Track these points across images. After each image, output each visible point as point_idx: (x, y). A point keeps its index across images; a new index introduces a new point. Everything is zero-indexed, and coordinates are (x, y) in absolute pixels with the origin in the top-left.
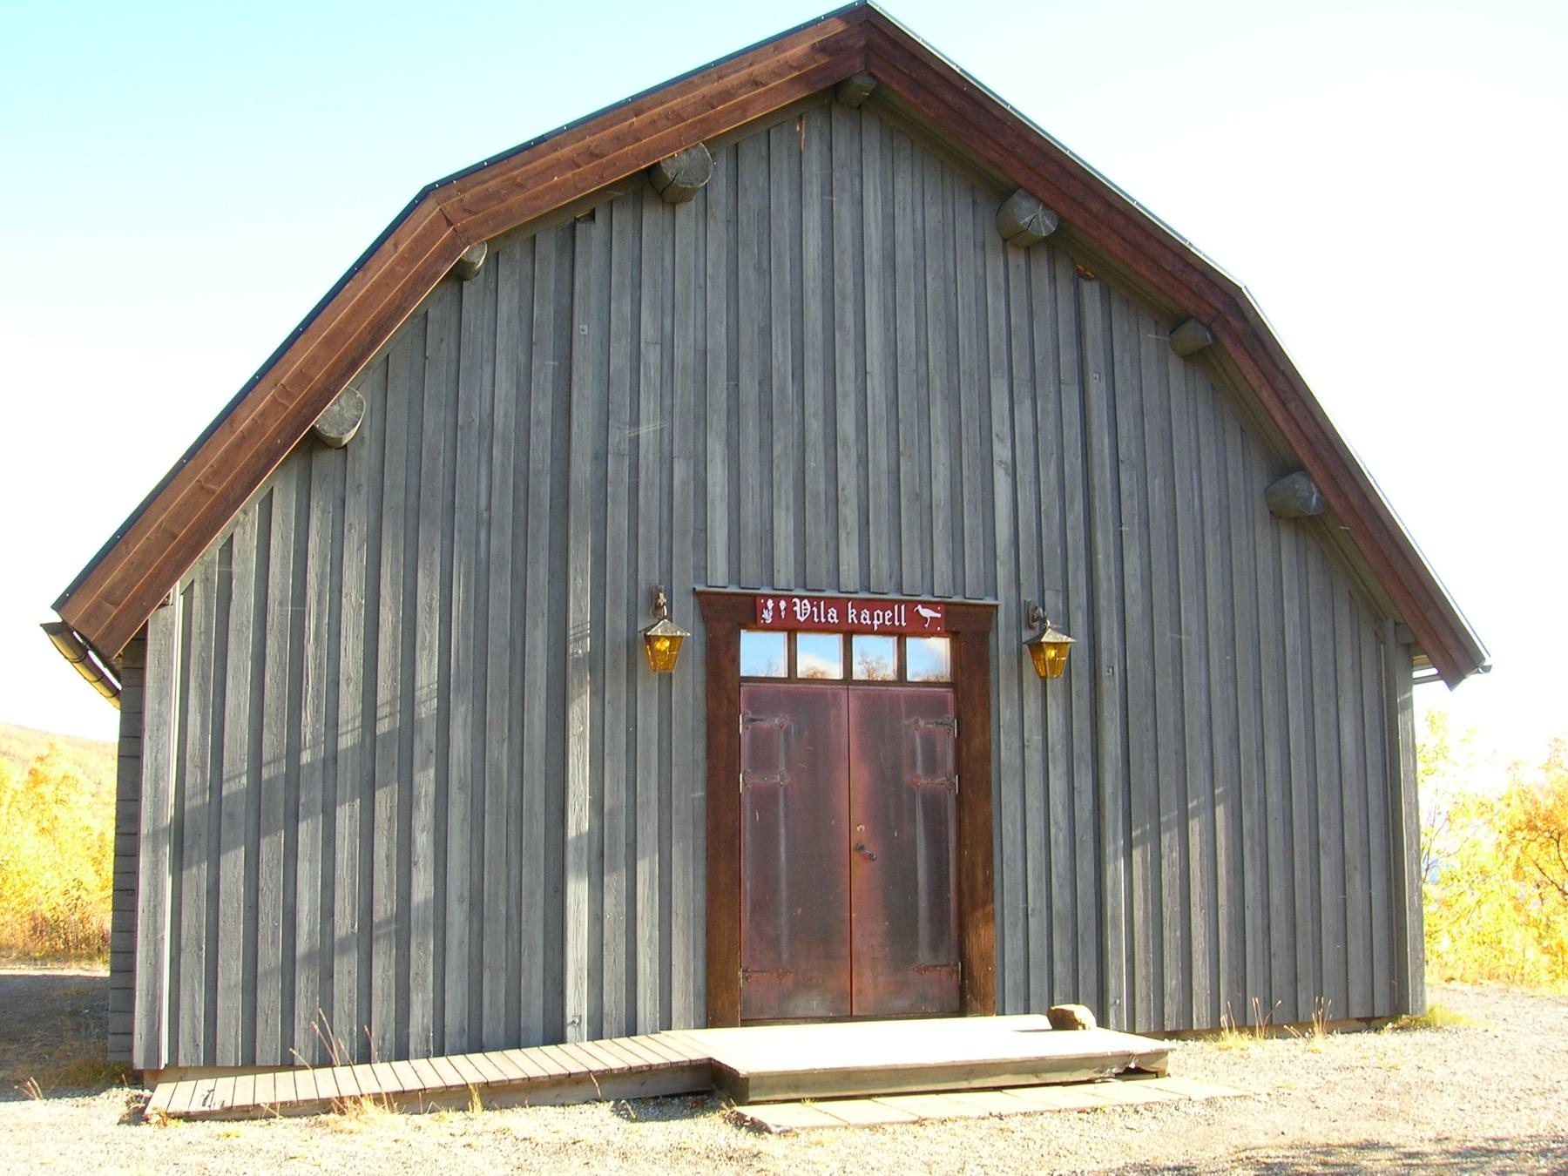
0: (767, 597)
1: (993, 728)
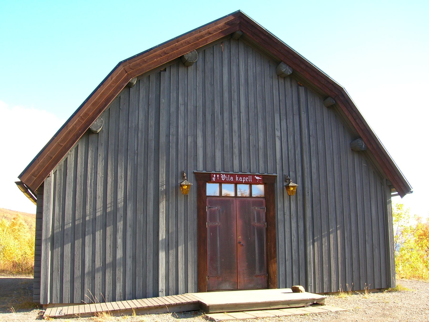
0: (214, 174)
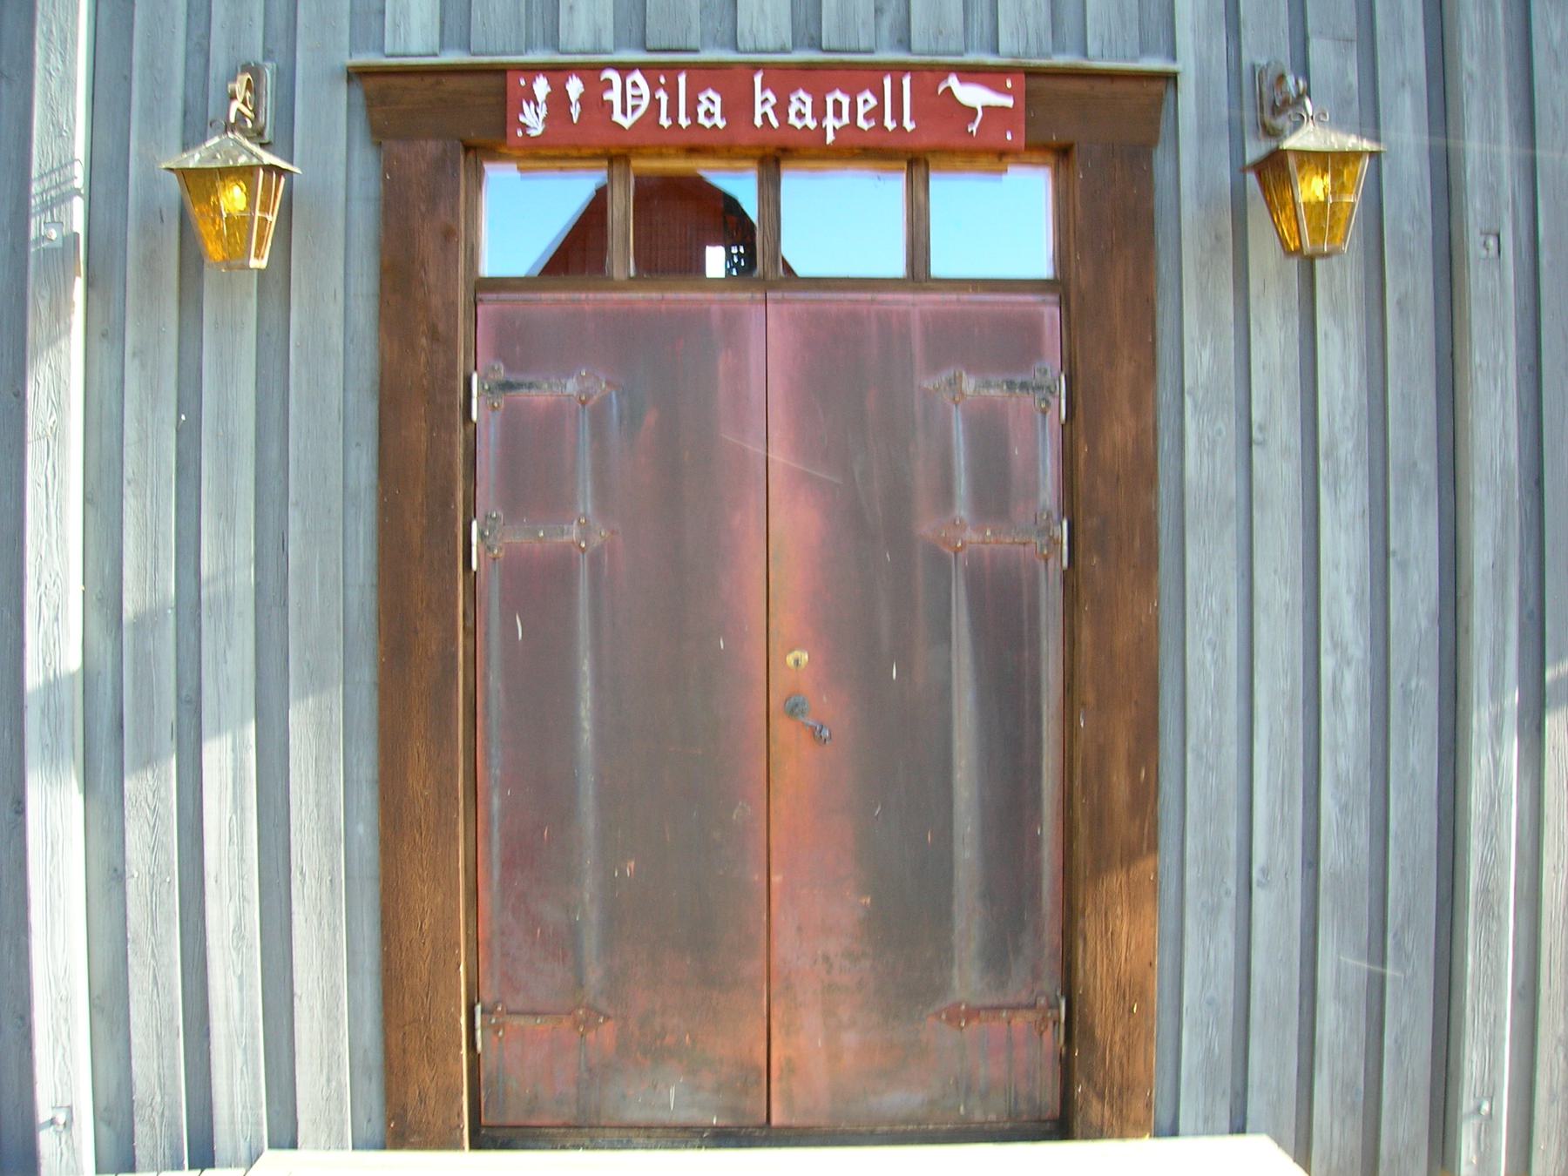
0: (533, 70)
1: (1165, 395)
